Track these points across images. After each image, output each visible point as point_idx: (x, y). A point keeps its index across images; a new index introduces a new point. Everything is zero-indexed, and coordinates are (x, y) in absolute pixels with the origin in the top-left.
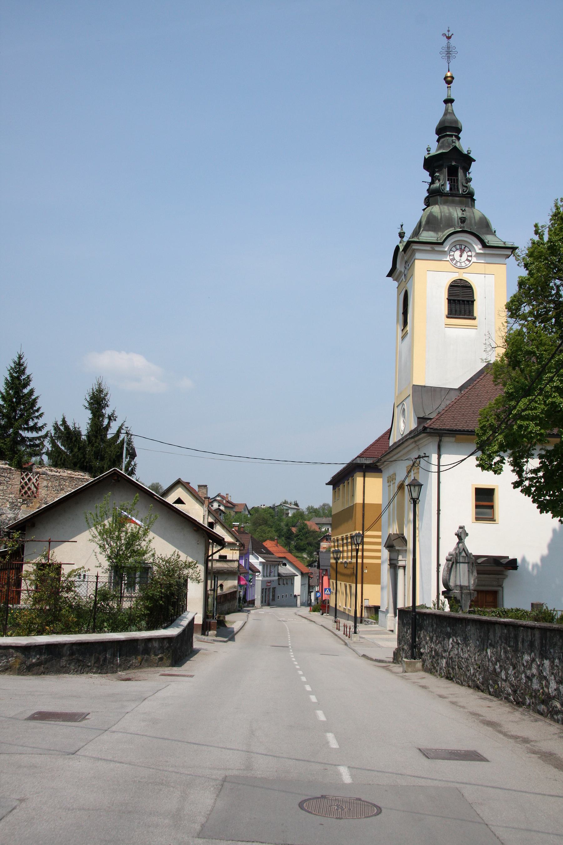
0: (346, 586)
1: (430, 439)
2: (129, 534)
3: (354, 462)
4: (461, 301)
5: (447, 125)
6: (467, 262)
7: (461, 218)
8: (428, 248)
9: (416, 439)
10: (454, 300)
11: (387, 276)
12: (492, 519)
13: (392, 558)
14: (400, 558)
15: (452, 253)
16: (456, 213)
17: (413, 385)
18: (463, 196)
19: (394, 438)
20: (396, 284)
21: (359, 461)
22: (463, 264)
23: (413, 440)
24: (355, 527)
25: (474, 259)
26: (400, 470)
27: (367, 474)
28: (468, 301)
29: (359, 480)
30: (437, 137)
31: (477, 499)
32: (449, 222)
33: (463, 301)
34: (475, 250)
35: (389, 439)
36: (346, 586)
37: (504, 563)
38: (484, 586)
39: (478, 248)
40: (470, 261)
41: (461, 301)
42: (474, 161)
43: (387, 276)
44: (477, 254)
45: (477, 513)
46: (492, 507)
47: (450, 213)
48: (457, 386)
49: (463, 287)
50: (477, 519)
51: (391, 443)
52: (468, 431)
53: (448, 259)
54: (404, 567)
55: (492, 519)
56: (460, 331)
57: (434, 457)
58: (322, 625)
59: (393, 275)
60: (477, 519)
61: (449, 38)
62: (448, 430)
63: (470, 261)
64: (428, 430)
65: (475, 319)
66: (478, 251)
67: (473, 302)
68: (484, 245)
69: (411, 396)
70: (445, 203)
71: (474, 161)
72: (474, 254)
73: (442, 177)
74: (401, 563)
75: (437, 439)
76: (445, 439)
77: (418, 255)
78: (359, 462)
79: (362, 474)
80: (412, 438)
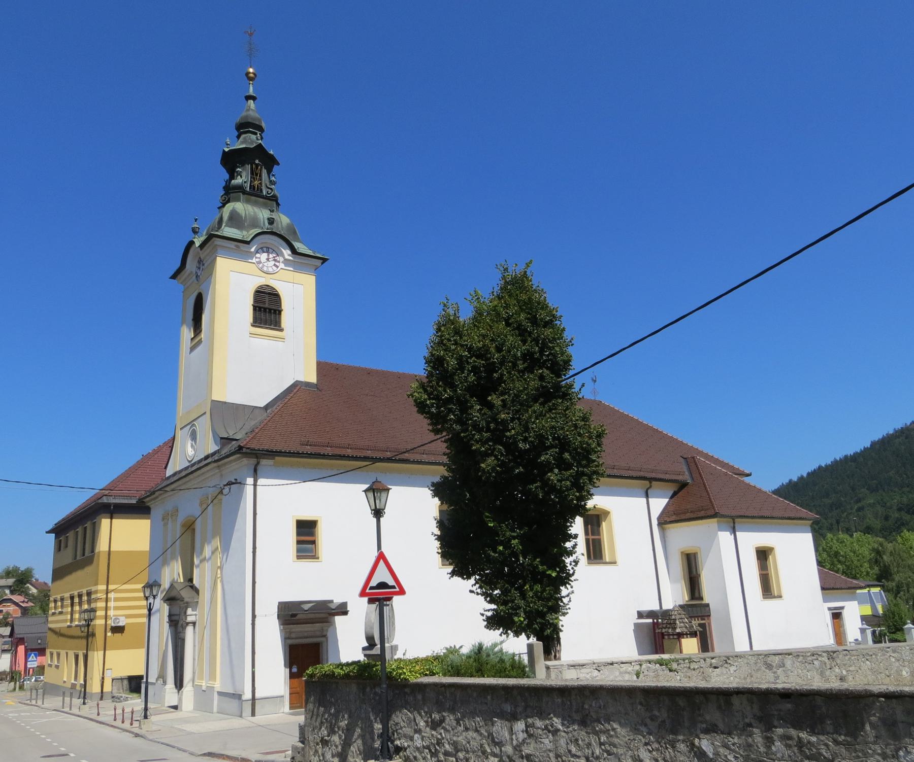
0: (77, 657)
1: (245, 461)
2: (849, 739)
3: (100, 501)
4: (267, 309)
5: (250, 120)
6: (275, 268)
7: (268, 219)
8: (232, 245)
9: (220, 463)
10: (260, 308)
11: (171, 278)
12: (315, 557)
13: (174, 612)
14: (189, 611)
15: (258, 255)
16: (263, 214)
17: (213, 401)
18: (266, 198)
19: (176, 464)
20: (182, 287)
21: (105, 500)
22: (270, 270)
23: (215, 464)
24: (97, 580)
25: (282, 266)
26: (187, 503)
27: (114, 515)
28: (275, 311)
29: (105, 523)
30: (237, 134)
31: (298, 534)
32: (254, 223)
33: (270, 310)
34: (283, 256)
35: (166, 468)
36: (77, 657)
37: (306, 608)
38: (307, 637)
39: (287, 253)
40: (277, 267)
41: (267, 309)
42: (278, 164)
43: (171, 278)
44: (285, 260)
45: (298, 551)
46: (313, 542)
47: (255, 213)
48: (262, 404)
49: (269, 294)
50: (299, 557)
51: (169, 472)
52: (289, 453)
53: (254, 260)
54: (194, 624)
55: (315, 557)
56: (264, 342)
57: (250, 481)
58: (204, 755)
59: (179, 276)
60: (299, 557)
61: (251, 35)
62: (267, 451)
63: (277, 267)
64: (244, 450)
65: (282, 330)
66: (287, 257)
67: (280, 312)
68: (294, 251)
69: (208, 414)
70: (248, 201)
71: (278, 164)
72: (281, 259)
73: (244, 174)
74: (189, 619)
75: (253, 461)
76: (264, 462)
77: (219, 251)
78: (106, 501)
79: (109, 515)
80: (216, 461)
